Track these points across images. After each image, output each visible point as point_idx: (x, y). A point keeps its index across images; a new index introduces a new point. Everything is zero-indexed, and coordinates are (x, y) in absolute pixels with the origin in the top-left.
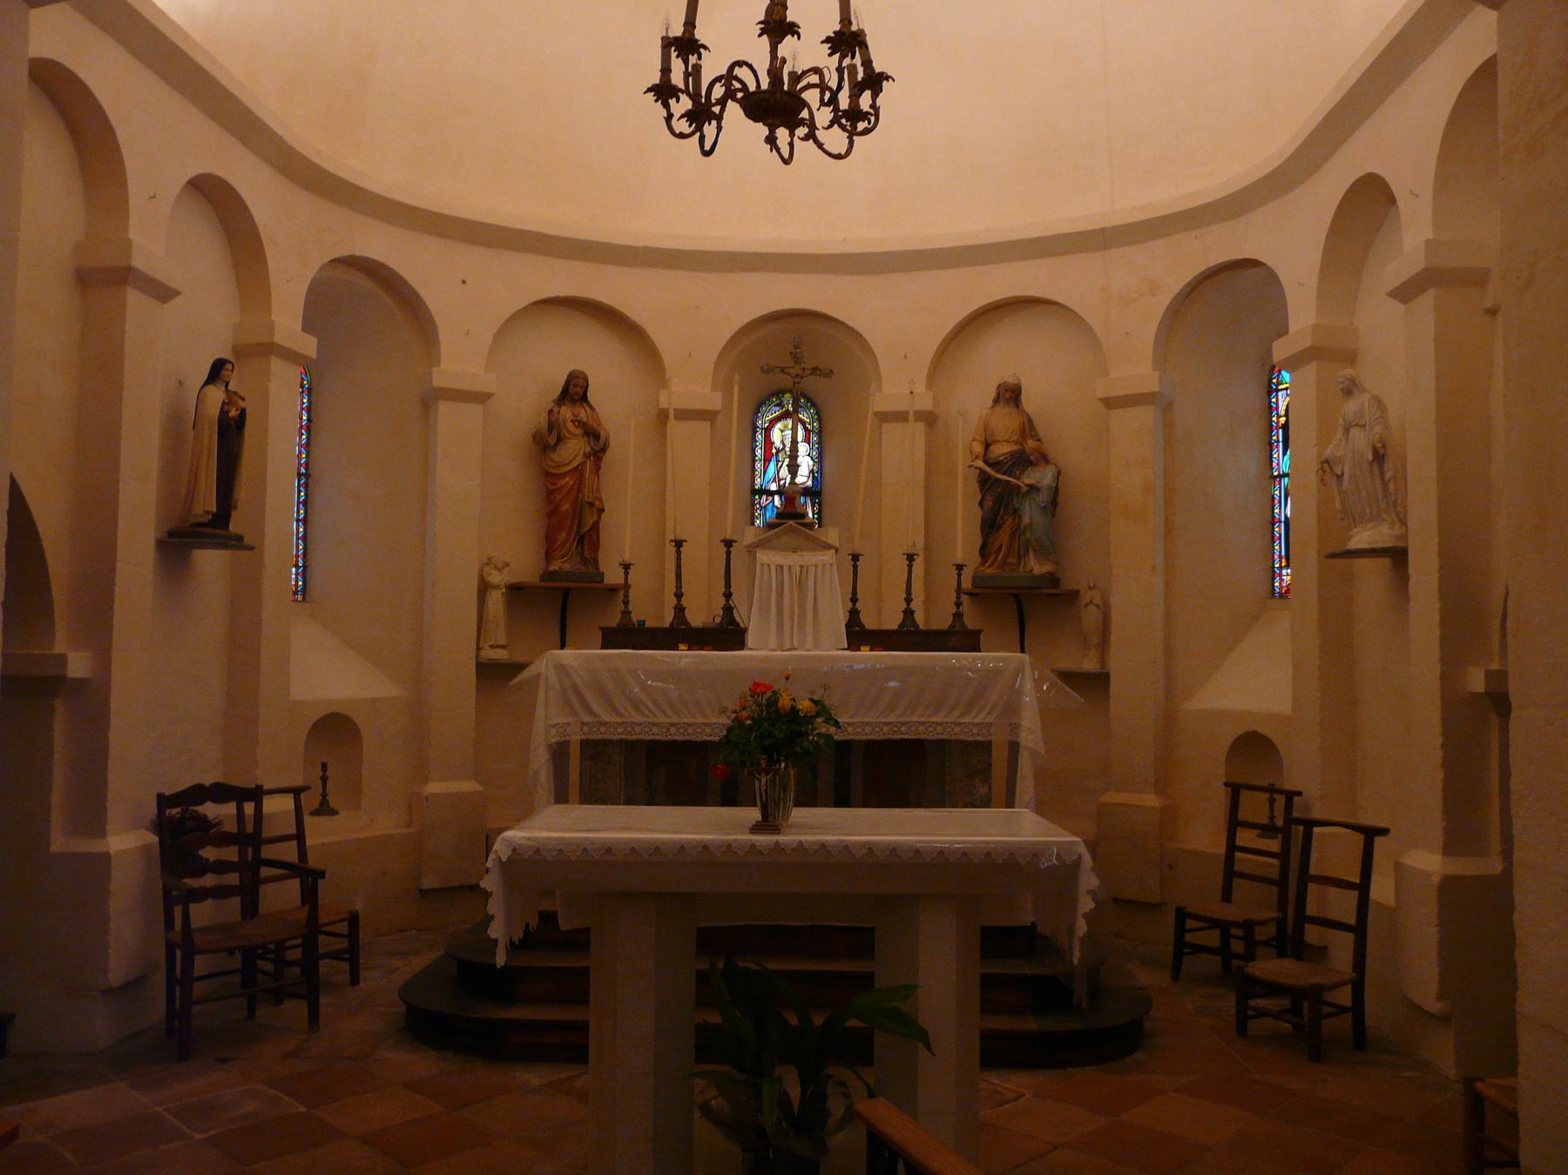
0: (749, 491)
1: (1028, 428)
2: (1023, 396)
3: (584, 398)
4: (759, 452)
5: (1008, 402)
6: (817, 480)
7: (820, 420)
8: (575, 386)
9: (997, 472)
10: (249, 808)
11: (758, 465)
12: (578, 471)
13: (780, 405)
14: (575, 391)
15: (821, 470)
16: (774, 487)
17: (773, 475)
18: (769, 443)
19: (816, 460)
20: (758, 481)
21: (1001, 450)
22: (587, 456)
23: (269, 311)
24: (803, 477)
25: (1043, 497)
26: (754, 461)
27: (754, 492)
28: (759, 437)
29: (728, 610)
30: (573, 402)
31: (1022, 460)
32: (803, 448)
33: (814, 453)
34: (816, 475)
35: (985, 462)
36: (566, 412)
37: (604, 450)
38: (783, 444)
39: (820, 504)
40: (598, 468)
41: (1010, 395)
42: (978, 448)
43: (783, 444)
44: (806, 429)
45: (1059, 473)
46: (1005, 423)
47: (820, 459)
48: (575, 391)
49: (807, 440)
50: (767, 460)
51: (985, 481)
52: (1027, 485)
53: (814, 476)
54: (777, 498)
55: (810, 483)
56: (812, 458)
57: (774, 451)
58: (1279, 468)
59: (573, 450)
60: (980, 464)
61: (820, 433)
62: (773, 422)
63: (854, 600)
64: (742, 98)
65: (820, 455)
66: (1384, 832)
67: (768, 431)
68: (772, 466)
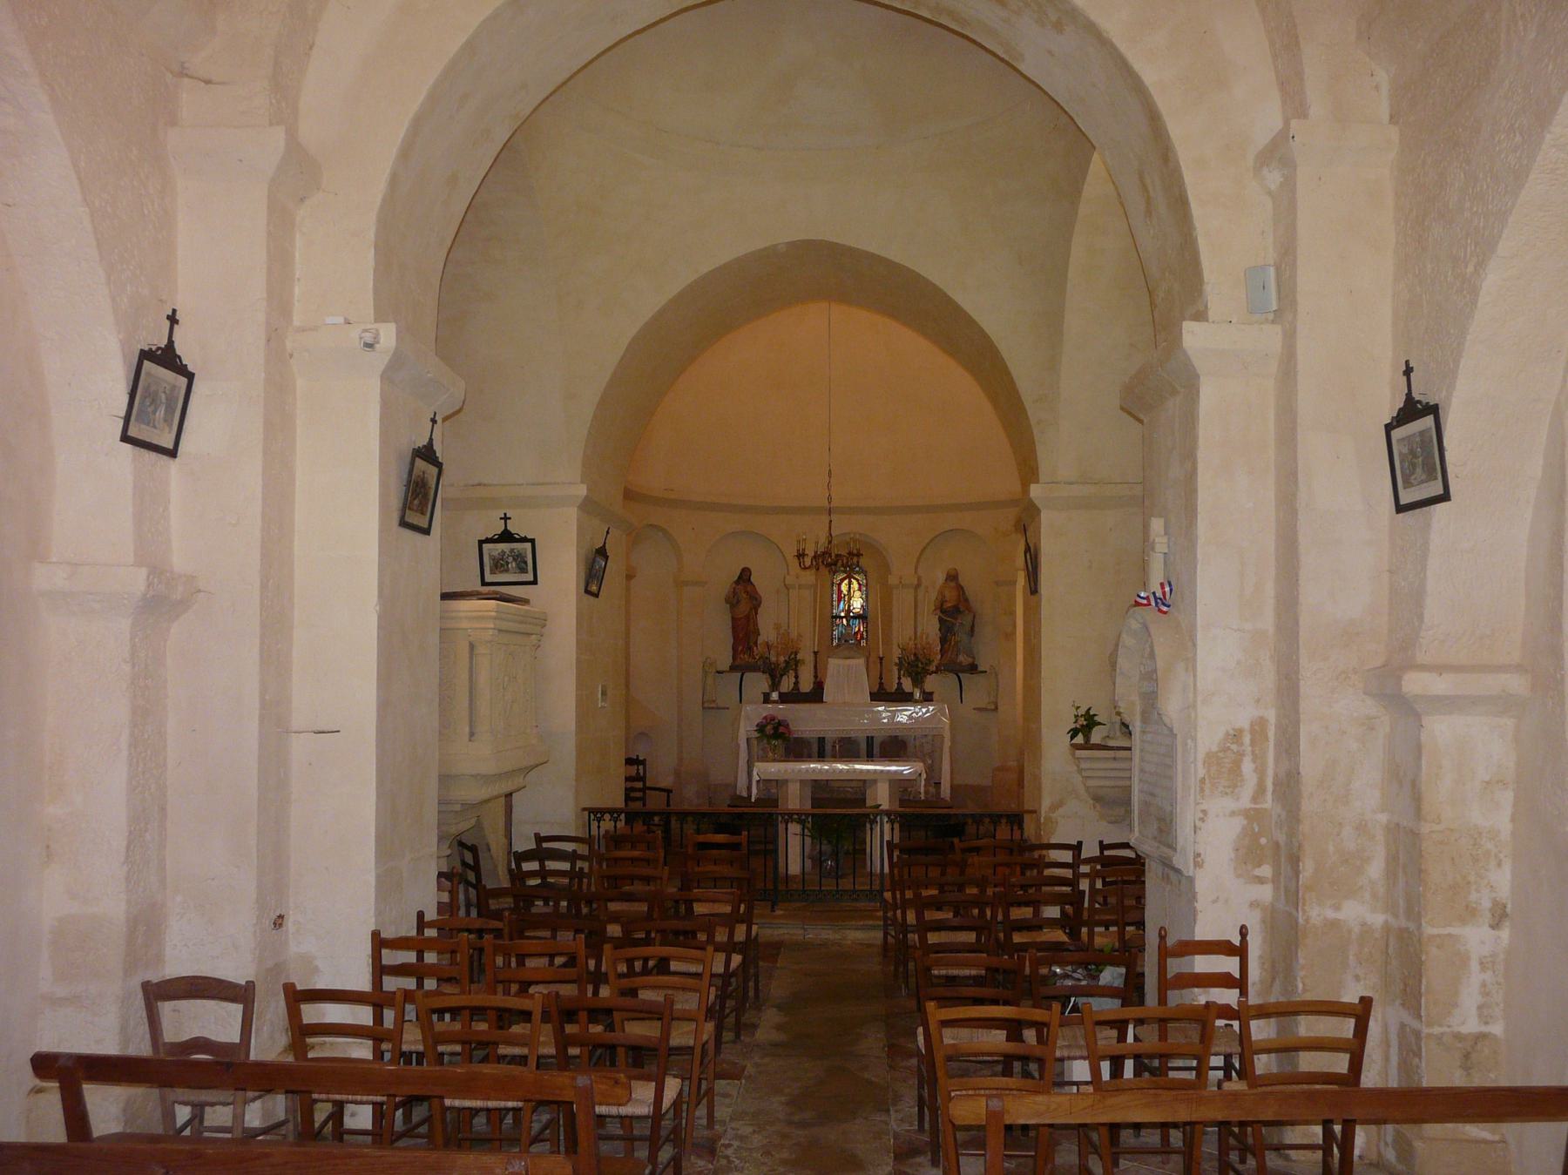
0: (646, 955)
1: (960, 588)
10: (641, 767)
12: (747, 618)
14: (745, 577)
16: (843, 614)
18: (840, 591)
23: (524, 1022)
26: (832, 601)
27: (833, 617)
29: (431, 439)
35: (941, 611)
37: (759, 605)
40: (756, 614)
41: (952, 577)
45: (974, 617)
46: (951, 595)
47: (866, 600)
48: (745, 577)
50: (839, 601)
54: (844, 620)
57: (670, 904)
58: (611, 1123)
59: (744, 608)
62: (842, 580)
63: (881, 678)
65: (867, 597)
66: (1101, 842)
67: (840, 585)
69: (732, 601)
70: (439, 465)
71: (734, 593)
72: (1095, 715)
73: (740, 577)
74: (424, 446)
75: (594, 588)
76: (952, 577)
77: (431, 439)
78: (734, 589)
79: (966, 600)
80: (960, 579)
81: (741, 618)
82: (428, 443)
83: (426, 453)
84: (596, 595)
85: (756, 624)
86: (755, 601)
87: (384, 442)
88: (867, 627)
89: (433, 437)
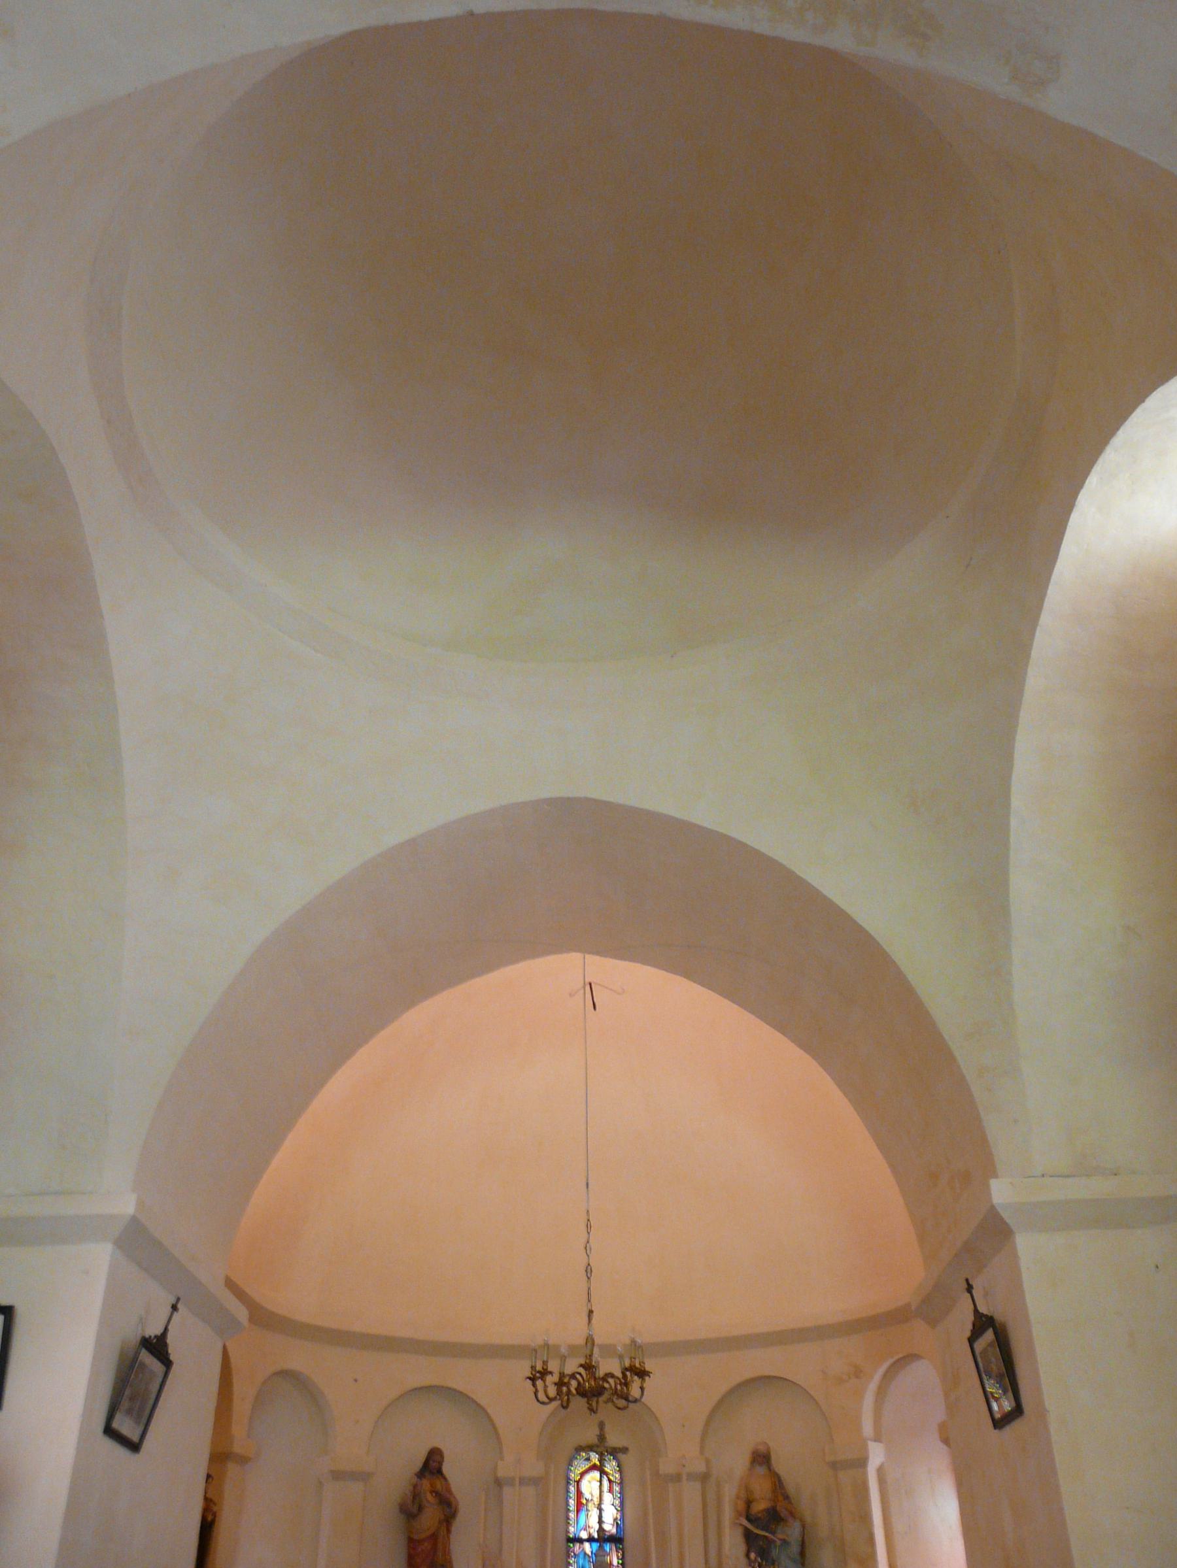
1: (778, 1483)
2: (773, 1457)
3: (439, 1472)
4: (572, 1502)
5: (761, 1464)
6: (620, 1528)
7: (620, 1471)
8: (434, 1461)
9: (757, 1527)
11: (572, 1515)
12: (434, 1537)
13: (588, 1459)
14: (432, 1465)
15: (623, 1518)
17: (587, 1524)
19: (619, 1509)
20: (572, 1529)
21: (760, 1507)
22: (440, 1522)
24: (609, 1527)
25: (795, 1549)
28: (572, 1489)
29: (166, 1329)
30: (432, 1473)
31: (774, 1518)
32: (608, 1497)
33: (617, 1502)
34: (619, 1522)
35: (748, 1519)
36: (426, 1484)
38: (592, 1495)
39: (622, 1549)
40: (449, 1531)
41: (761, 1458)
42: (741, 1505)
43: (592, 1495)
44: (610, 1481)
45: (804, 1527)
46: (762, 1489)
47: (622, 1508)
48: (432, 1465)
49: (611, 1491)
51: (749, 1536)
52: (781, 1540)
53: (617, 1523)
55: (614, 1531)
56: (615, 1507)
59: (430, 1518)
60: (745, 1523)
61: (621, 1484)
62: (582, 1474)
64: (620, 1544)
68: (583, 1515)
69: (410, 1510)
70: (167, 1363)
71: (416, 1494)
72: (650, 1377)
73: (426, 1464)
74: (156, 1337)
75: (126, 1426)
76: (761, 1458)
77: (166, 1329)
78: (415, 1486)
79: (787, 1497)
80: (773, 1461)
81: (423, 1540)
82: (162, 1334)
83: (157, 1347)
84: (134, 1447)
85: (447, 1552)
86: (448, 1508)
87: (105, 1322)
88: (623, 1558)
89: (170, 1327)
